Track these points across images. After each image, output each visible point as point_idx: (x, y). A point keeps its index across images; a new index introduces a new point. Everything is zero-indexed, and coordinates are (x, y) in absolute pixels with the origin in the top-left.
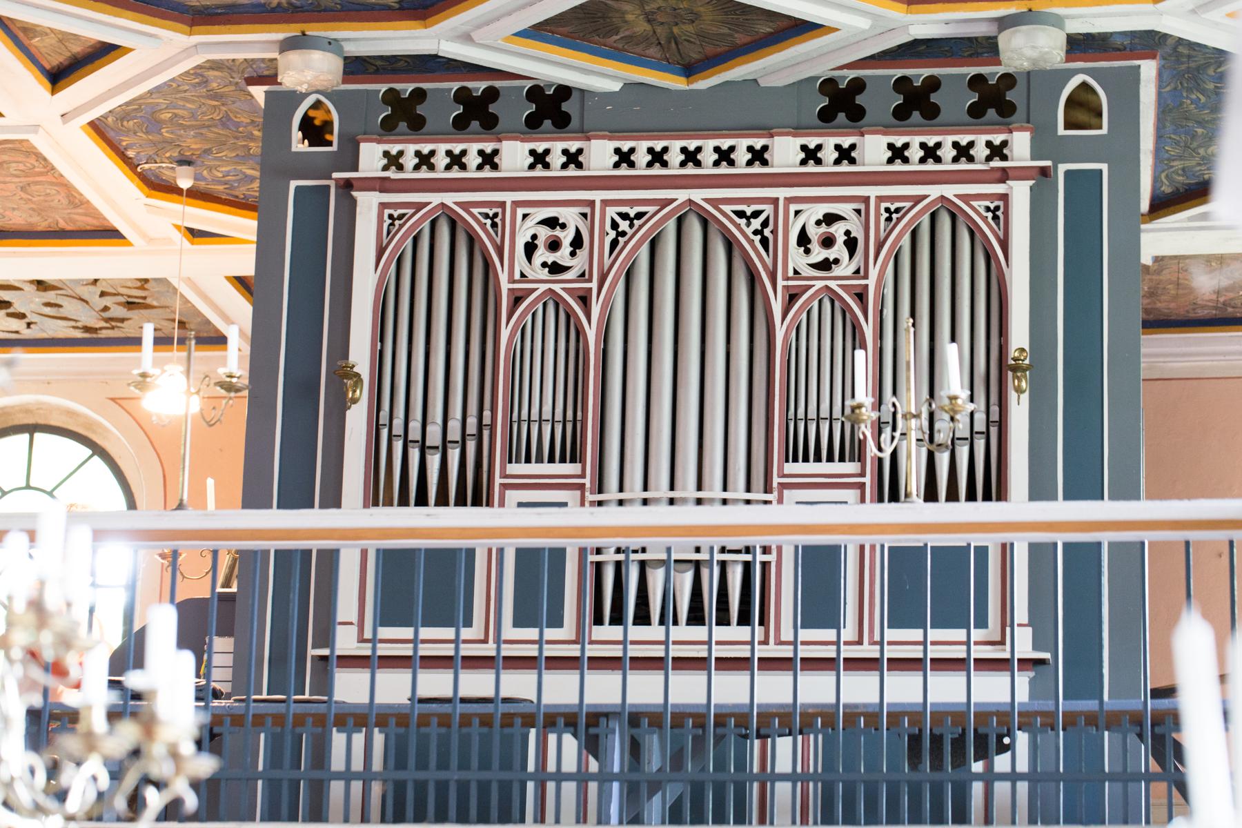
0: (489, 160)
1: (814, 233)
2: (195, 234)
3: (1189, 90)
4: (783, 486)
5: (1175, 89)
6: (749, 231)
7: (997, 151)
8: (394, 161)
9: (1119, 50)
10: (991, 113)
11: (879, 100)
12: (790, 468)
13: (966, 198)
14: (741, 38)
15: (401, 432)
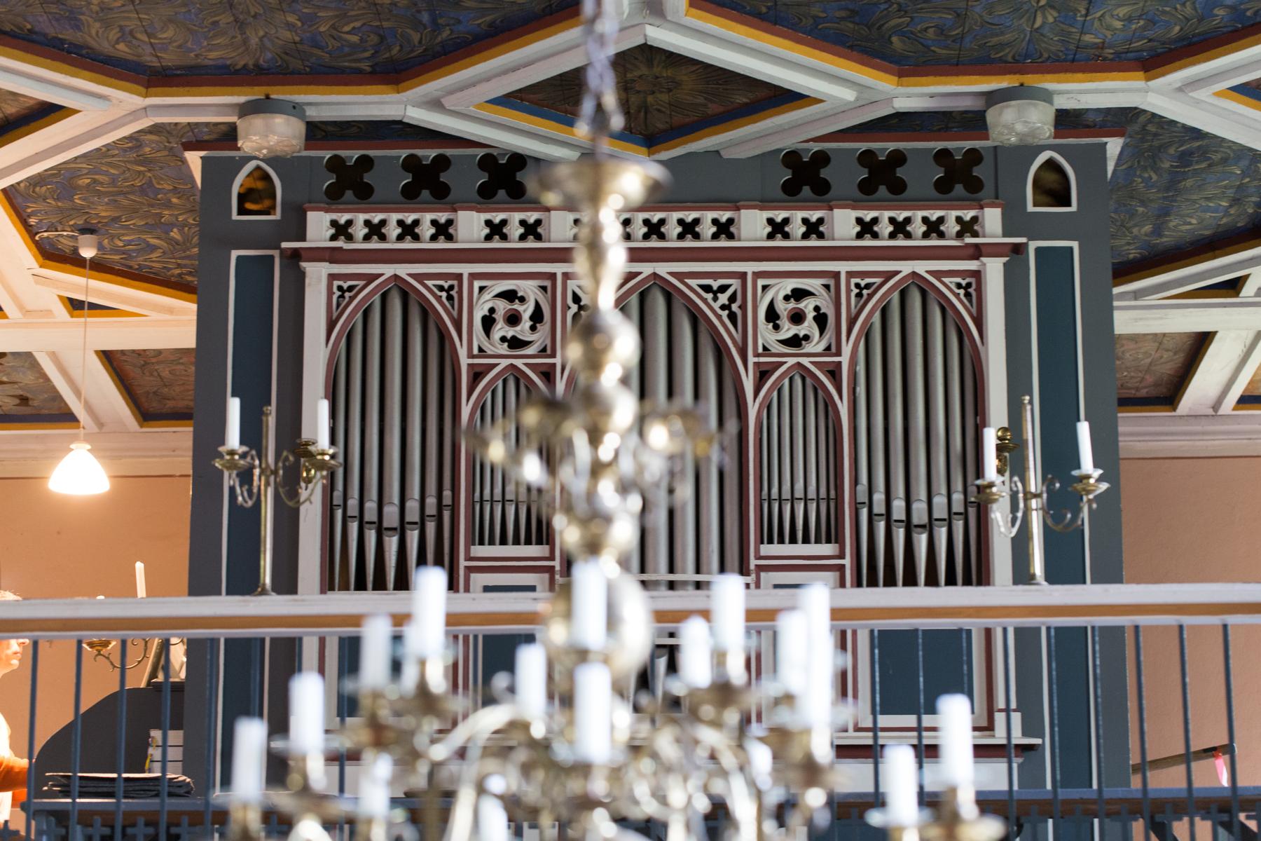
0: (443, 230)
1: (783, 308)
2: (75, 306)
3: (1145, 169)
4: (760, 568)
5: (1130, 167)
6: (716, 306)
7: (968, 227)
8: (341, 230)
9: (1088, 126)
10: (959, 189)
11: (844, 175)
12: (766, 549)
13: (938, 274)
14: (713, 108)
15: (356, 513)
